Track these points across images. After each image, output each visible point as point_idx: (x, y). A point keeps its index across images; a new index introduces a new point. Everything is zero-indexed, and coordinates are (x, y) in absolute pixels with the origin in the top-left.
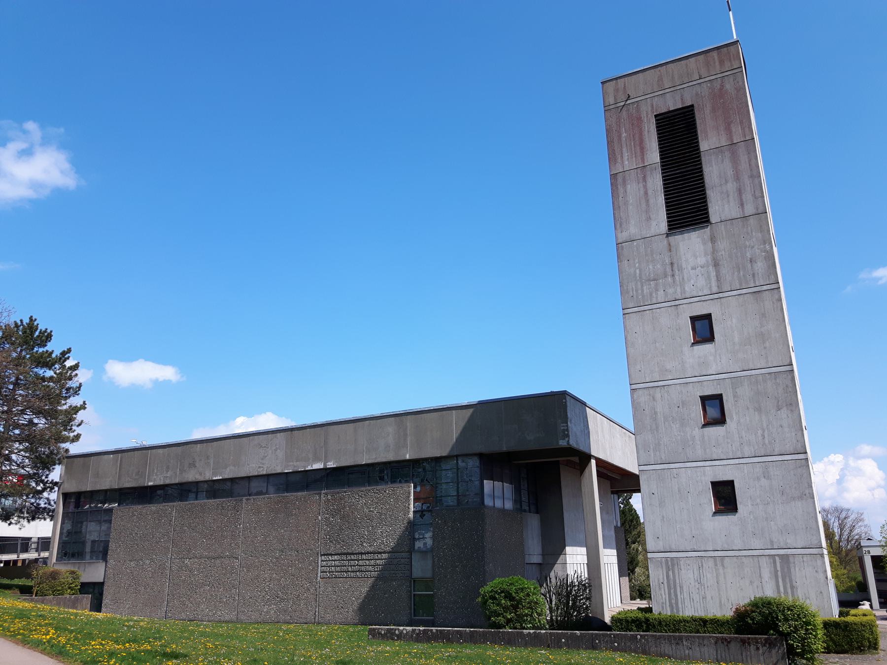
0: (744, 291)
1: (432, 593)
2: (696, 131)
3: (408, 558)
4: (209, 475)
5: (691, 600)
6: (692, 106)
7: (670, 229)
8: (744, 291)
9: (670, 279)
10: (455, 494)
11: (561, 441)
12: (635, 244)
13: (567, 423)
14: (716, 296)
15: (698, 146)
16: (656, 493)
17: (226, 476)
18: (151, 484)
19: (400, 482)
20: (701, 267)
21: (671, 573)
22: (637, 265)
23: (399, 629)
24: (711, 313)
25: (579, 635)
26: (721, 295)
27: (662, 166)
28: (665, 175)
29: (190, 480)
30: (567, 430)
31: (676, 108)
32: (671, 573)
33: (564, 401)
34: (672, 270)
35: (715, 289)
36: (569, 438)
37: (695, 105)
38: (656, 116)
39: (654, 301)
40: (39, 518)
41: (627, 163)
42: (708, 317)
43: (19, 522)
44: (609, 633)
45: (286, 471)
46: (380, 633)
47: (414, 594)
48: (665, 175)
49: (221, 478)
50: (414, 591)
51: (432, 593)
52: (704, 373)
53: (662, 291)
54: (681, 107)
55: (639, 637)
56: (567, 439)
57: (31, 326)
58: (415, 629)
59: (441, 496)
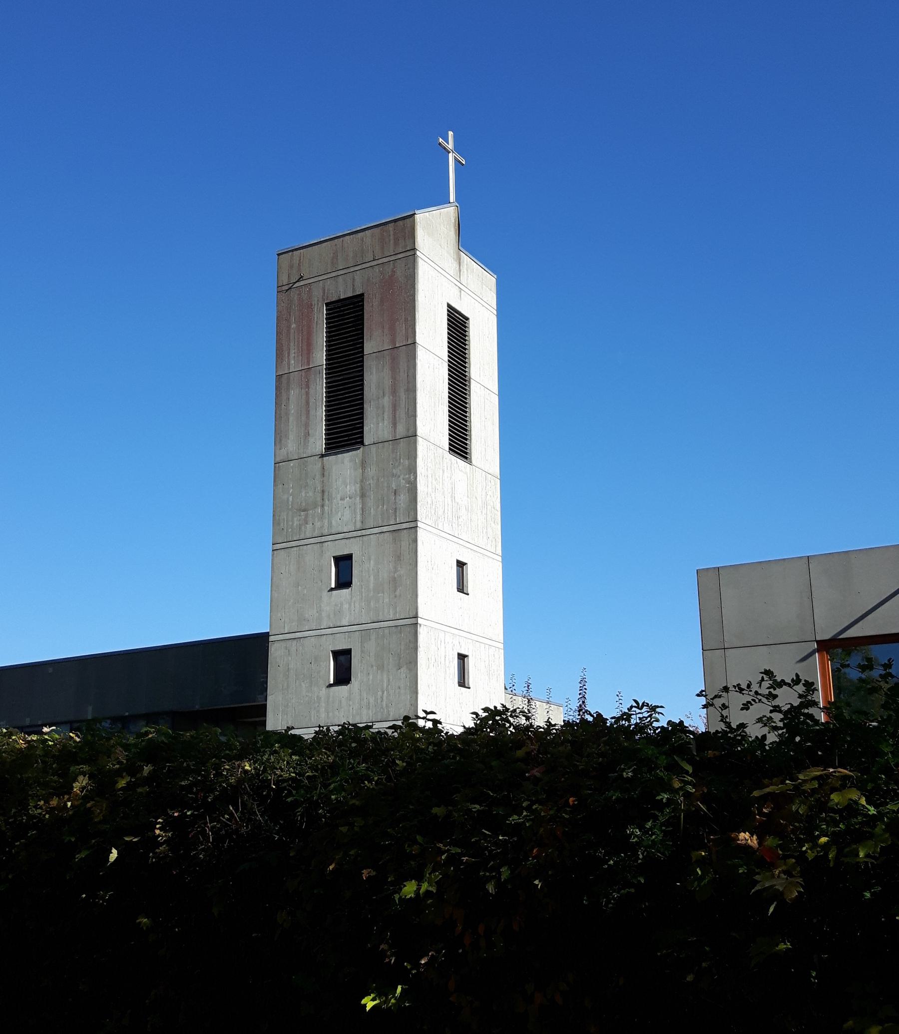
8: (385, 529)
52: (338, 624)
53: (311, 525)
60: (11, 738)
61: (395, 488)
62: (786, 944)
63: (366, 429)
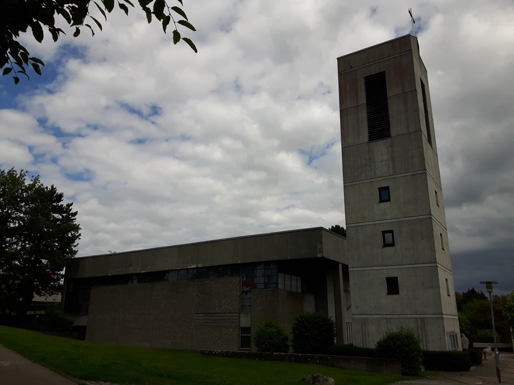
0: (407, 174)
1: (250, 335)
2: (386, 86)
3: (238, 316)
4: (138, 271)
5: (374, 341)
6: (384, 72)
7: (369, 140)
8: (407, 174)
9: (368, 167)
10: (263, 282)
11: (319, 254)
12: (351, 148)
13: (322, 245)
14: (392, 177)
15: (386, 94)
16: (357, 283)
17: (147, 271)
18: (110, 275)
19: (235, 275)
20: (385, 161)
21: (363, 326)
22: (352, 160)
23: (214, 351)
24: (389, 186)
25: (300, 356)
26: (395, 176)
27: (367, 105)
28: (368, 110)
29: (129, 273)
30: (322, 249)
31: (375, 73)
32: (363, 326)
33: (321, 232)
34: (370, 162)
35: (392, 173)
36: (323, 253)
37: (386, 71)
38: (365, 78)
39: (360, 180)
40: (55, 293)
41: (349, 104)
42: (387, 188)
43: (45, 295)
44: (315, 355)
45: (178, 269)
46: (205, 353)
47: (241, 336)
48: (368, 110)
49: (145, 272)
50: (241, 334)
51: (250, 335)
52: (384, 219)
53: (364, 174)
54: (378, 72)
55: (329, 357)
56: (322, 253)
57: (53, 190)
58: (222, 351)
59: (256, 284)
60: (36, 206)
61: (411, 155)
62: (40, 184)
63: (391, 130)
